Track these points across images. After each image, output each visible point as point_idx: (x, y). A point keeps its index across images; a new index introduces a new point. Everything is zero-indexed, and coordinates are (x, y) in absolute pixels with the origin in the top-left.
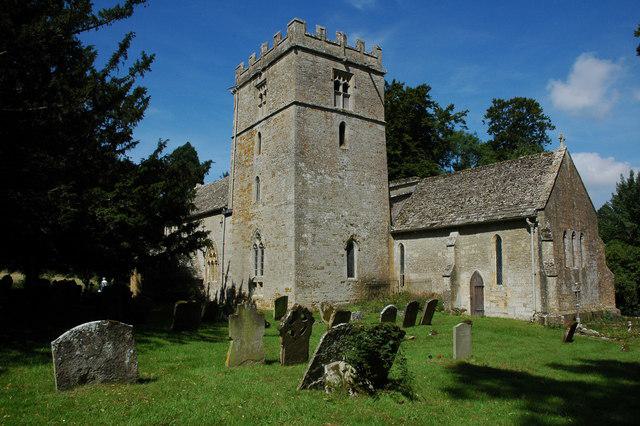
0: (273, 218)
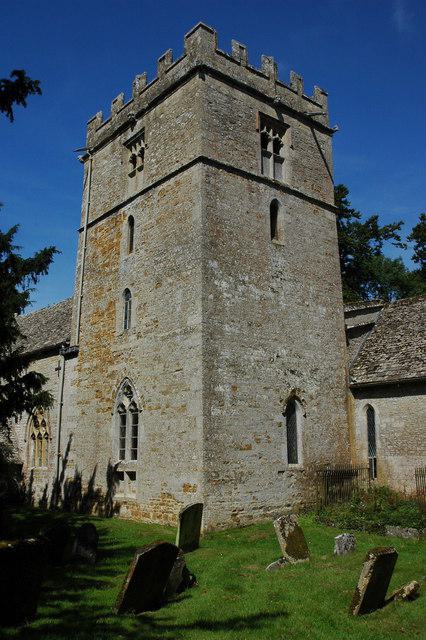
0: (157, 359)
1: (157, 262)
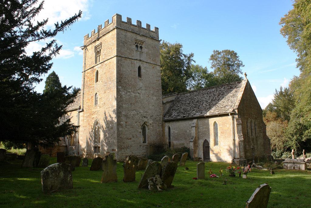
1: (105, 86)
